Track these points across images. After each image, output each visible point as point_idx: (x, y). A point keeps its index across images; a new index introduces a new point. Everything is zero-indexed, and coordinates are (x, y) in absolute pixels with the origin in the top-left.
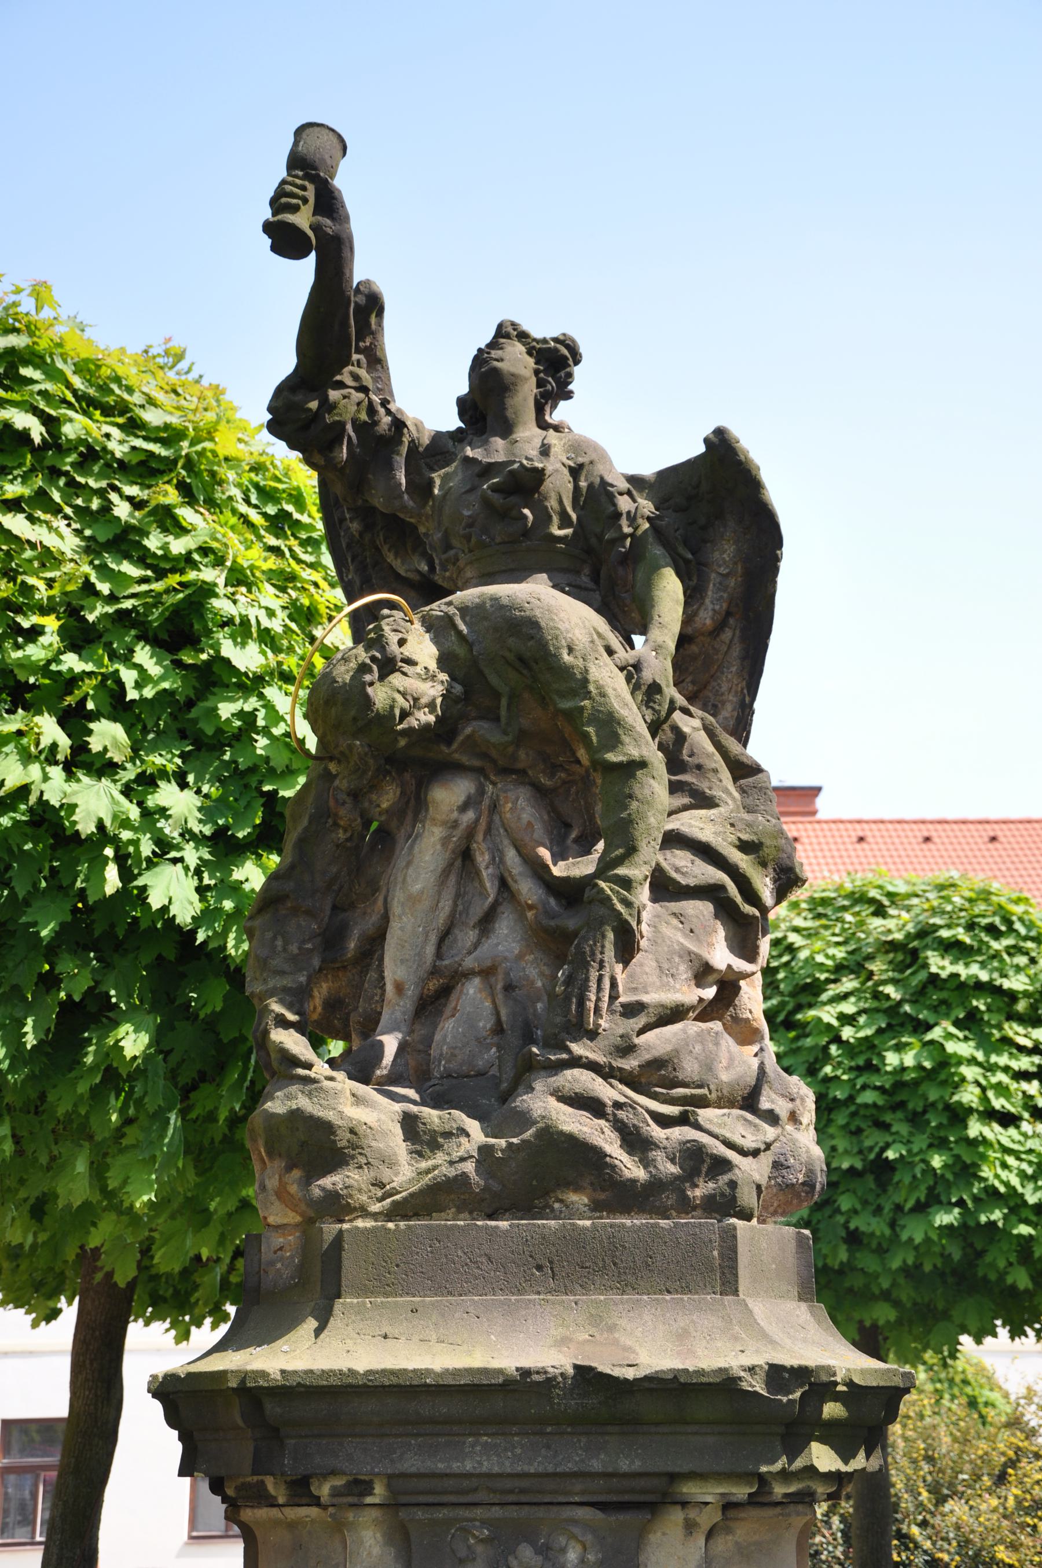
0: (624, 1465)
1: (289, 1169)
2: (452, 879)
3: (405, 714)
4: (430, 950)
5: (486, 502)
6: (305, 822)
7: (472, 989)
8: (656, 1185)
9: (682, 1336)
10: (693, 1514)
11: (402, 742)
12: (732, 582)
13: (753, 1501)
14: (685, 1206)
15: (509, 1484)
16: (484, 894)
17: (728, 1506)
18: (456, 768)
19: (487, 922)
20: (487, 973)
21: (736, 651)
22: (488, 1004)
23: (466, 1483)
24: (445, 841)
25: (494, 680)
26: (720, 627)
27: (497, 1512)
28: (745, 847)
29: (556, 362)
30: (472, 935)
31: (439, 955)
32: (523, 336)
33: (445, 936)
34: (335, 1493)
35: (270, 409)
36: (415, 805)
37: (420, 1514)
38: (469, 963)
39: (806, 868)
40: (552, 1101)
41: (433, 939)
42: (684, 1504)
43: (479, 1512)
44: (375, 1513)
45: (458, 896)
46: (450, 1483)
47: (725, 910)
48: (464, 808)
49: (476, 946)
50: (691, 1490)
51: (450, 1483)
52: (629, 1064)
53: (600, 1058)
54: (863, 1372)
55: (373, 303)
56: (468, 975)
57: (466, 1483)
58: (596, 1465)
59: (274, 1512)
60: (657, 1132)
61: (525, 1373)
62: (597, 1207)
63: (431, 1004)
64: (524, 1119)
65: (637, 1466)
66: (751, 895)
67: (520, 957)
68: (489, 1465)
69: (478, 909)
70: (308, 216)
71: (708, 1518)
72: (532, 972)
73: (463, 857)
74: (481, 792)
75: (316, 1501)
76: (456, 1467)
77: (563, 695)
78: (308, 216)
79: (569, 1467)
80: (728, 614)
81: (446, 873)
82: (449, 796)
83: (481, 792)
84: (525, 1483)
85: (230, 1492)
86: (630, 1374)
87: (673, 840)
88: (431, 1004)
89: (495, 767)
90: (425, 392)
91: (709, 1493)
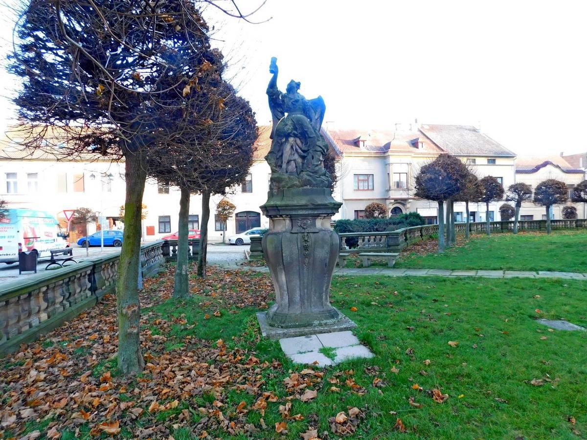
7: (292, 162)
18: (291, 136)
36: (287, 140)
70: (274, 70)
73: (292, 147)
78: (274, 70)
82: (291, 139)
88: (289, 162)
89: (295, 136)
90: (282, 87)
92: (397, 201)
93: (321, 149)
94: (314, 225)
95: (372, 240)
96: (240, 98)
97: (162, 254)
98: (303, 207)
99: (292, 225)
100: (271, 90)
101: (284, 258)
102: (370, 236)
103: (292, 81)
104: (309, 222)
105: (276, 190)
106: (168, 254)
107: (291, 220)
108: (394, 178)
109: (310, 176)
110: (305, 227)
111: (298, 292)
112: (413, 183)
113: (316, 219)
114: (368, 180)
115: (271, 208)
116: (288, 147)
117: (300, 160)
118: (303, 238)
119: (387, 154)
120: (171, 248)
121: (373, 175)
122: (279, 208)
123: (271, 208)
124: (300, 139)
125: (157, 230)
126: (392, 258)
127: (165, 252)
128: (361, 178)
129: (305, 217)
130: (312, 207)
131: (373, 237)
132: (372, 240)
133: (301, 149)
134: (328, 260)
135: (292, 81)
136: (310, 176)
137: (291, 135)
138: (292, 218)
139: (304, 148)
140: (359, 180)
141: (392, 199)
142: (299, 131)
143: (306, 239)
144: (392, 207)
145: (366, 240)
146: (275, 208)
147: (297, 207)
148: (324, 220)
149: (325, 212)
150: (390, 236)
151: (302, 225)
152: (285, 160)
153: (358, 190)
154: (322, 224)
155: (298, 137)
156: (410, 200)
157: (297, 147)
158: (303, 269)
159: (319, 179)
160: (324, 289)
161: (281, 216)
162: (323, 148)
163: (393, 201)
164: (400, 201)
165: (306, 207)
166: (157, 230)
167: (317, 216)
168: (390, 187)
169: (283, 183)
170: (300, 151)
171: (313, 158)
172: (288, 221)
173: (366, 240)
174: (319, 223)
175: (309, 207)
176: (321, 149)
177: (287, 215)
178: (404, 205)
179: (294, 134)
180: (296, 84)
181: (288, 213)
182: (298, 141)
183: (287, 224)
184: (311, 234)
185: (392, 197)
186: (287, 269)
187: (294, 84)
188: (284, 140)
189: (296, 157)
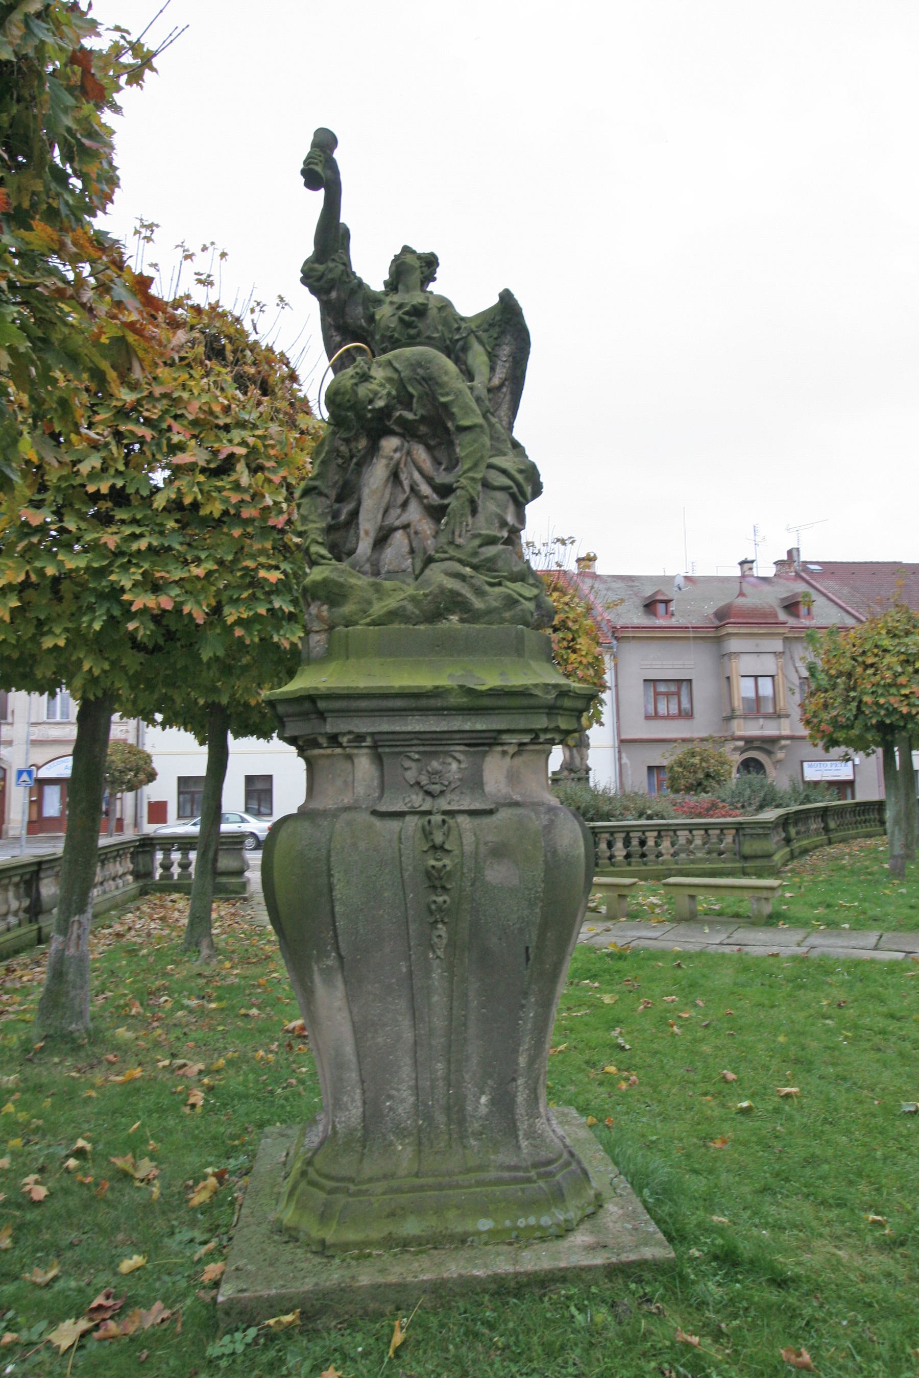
0: (479, 727)
1: (323, 605)
2: (390, 485)
3: (371, 402)
4: (380, 516)
5: (401, 320)
6: (323, 455)
7: (399, 535)
8: (489, 612)
9: (502, 674)
10: (505, 748)
11: (369, 415)
12: (507, 365)
13: (533, 742)
14: (502, 621)
15: (428, 736)
16: (404, 492)
17: (521, 744)
18: (392, 433)
19: (405, 505)
20: (406, 527)
21: (508, 398)
22: (406, 541)
23: (408, 736)
24: (387, 466)
25: (410, 389)
26: (502, 385)
27: (422, 749)
28: (521, 471)
29: (430, 263)
30: (399, 511)
31: (383, 521)
32: (414, 252)
33: (386, 511)
34: (349, 741)
35: (302, 271)
36: (373, 449)
37: (387, 750)
38: (397, 523)
39: (320, 686)
40: (442, 575)
41: (381, 511)
42: (502, 744)
43: (414, 749)
44: (365, 751)
45: (391, 494)
46: (401, 737)
47: (513, 496)
48: (395, 451)
49: (399, 516)
50: (506, 738)
51: (401, 737)
52: (475, 561)
53: (463, 557)
54: (580, 688)
55: (346, 234)
56: (396, 529)
57: (408, 736)
58: (467, 727)
59: (321, 751)
60: (487, 588)
61: (437, 687)
62: (462, 621)
63: (382, 540)
64: (428, 583)
65: (484, 728)
66: (523, 493)
67: (420, 521)
68: (418, 728)
69: (401, 498)
70: (321, 170)
71: (512, 750)
72: (426, 527)
73: (395, 476)
74: (403, 445)
75: (340, 745)
76: (404, 729)
77: (443, 395)
78: (321, 170)
79: (455, 728)
80: (506, 379)
81: (387, 480)
82: (390, 444)
83: (403, 445)
84: (434, 736)
85: (301, 743)
86: (484, 688)
87: (490, 466)
88: (382, 540)
89: (408, 431)
90: (371, 267)
91: (514, 739)
92: (750, 742)
93: (507, 482)
94: (475, 782)
95: (698, 842)
96: (588, 737)
97: (132, 873)
98: (424, 703)
99: (382, 776)
100: (320, 268)
101: (340, 924)
102: (691, 828)
103: (406, 250)
104: (454, 766)
105: (323, 637)
106: (149, 874)
107: (378, 759)
108: (745, 689)
109: (462, 578)
110: (436, 788)
111: (406, 1071)
112: (792, 703)
113: (485, 754)
114: (678, 694)
115: (290, 709)
116: (376, 475)
117: (426, 526)
118: (427, 834)
119: (724, 632)
120: (159, 856)
121: (690, 681)
122: (322, 705)
123: (290, 709)
124: (429, 448)
125: (172, 810)
126: (765, 894)
127: (141, 868)
128: (662, 688)
129: (435, 744)
130: (464, 701)
131: (698, 833)
132: (698, 842)
133: (429, 480)
134: (533, 936)
135: (406, 250)
136: (462, 578)
137: (390, 423)
138: (381, 748)
139: (442, 478)
140: (657, 694)
141: (740, 738)
142: (421, 412)
143: (438, 838)
144: (737, 758)
145: (682, 841)
146: (307, 705)
147: (399, 703)
148: (518, 761)
149: (521, 723)
150: (748, 831)
151: (424, 780)
152: (368, 525)
153: (656, 716)
154: (513, 778)
155: (421, 439)
156: (783, 742)
157: (417, 476)
158: (428, 971)
159: (497, 589)
160: (522, 1061)
161: (334, 739)
162: (520, 477)
163: (741, 743)
164: (756, 744)
165: (439, 703)
166: (172, 810)
167: (484, 743)
168: (733, 710)
169: (348, 609)
170: (425, 489)
171: (474, 512)
172: (364, 764)
173: (682, 841)
174: (496, 772)
175: (453, 701)
176: (507, 482)
177: (359, 738)
178: (769, 753)
179: (402, 421)
180: (420, 257)
181: (363, 726)
182: (421, 454)
183: (359, 774)
184: (462, 820)
185: (739, 733)
186: (351, 970)
187: (409, 259)
188: (363, 443)
189: (414, 513)
